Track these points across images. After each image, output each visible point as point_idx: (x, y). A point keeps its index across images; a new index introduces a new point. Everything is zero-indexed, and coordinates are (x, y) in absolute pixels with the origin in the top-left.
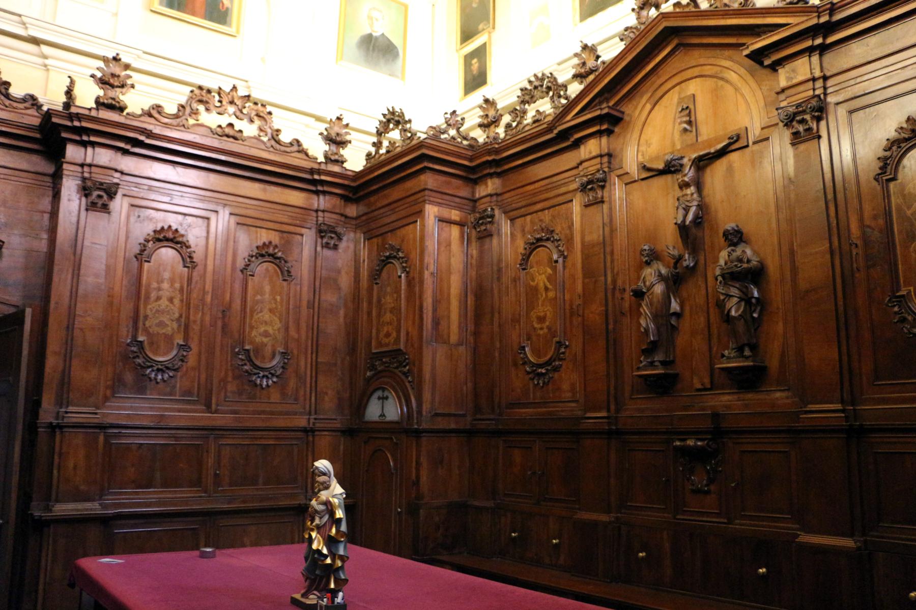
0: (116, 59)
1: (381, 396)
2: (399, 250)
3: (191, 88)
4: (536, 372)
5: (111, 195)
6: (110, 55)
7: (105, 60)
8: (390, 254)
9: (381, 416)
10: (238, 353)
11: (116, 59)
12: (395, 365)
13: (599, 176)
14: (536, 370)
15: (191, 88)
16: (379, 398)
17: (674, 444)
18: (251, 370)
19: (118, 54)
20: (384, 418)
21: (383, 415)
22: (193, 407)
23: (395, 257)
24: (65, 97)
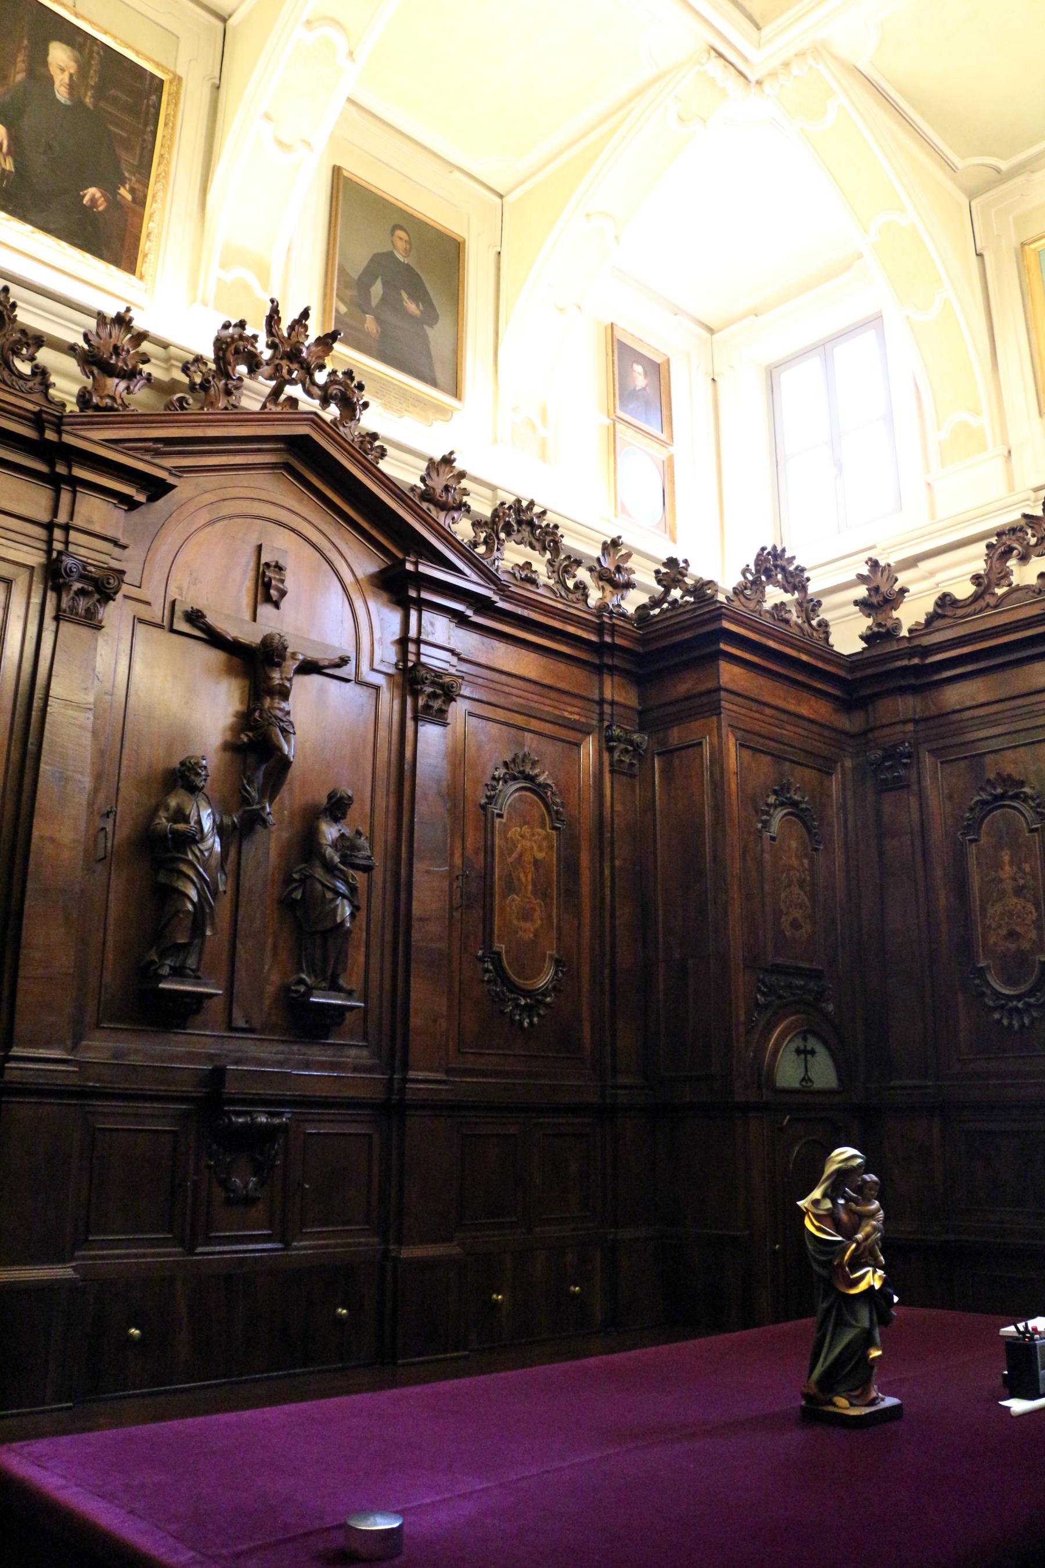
0: (122, 321)
1: (802, 1047)
2: (1022, 784)
3: (983, 544)
4: (1007, 1007)
5: (107, 597)
6: (111, 313)
7: (101, 317)
8: (1006, 792)
9: (804, 1079)
10: (481, 960)
11: (122, 321)
12: (765, 990)
13: (273, 592)
14: (1007, 1004)
15: (983, 544)
16: (798, 1052)
17: (495, 1296)
18: (504, 994)
19: (128, 310)
20: (809, 1084)
21: (806, 1079)
22: (779, 1029)
23: (1016, 797)
24: (440, 457)
